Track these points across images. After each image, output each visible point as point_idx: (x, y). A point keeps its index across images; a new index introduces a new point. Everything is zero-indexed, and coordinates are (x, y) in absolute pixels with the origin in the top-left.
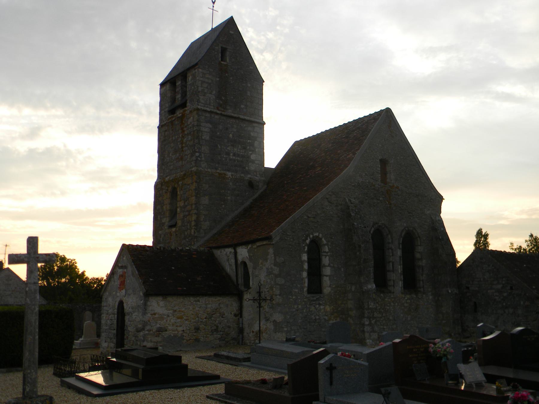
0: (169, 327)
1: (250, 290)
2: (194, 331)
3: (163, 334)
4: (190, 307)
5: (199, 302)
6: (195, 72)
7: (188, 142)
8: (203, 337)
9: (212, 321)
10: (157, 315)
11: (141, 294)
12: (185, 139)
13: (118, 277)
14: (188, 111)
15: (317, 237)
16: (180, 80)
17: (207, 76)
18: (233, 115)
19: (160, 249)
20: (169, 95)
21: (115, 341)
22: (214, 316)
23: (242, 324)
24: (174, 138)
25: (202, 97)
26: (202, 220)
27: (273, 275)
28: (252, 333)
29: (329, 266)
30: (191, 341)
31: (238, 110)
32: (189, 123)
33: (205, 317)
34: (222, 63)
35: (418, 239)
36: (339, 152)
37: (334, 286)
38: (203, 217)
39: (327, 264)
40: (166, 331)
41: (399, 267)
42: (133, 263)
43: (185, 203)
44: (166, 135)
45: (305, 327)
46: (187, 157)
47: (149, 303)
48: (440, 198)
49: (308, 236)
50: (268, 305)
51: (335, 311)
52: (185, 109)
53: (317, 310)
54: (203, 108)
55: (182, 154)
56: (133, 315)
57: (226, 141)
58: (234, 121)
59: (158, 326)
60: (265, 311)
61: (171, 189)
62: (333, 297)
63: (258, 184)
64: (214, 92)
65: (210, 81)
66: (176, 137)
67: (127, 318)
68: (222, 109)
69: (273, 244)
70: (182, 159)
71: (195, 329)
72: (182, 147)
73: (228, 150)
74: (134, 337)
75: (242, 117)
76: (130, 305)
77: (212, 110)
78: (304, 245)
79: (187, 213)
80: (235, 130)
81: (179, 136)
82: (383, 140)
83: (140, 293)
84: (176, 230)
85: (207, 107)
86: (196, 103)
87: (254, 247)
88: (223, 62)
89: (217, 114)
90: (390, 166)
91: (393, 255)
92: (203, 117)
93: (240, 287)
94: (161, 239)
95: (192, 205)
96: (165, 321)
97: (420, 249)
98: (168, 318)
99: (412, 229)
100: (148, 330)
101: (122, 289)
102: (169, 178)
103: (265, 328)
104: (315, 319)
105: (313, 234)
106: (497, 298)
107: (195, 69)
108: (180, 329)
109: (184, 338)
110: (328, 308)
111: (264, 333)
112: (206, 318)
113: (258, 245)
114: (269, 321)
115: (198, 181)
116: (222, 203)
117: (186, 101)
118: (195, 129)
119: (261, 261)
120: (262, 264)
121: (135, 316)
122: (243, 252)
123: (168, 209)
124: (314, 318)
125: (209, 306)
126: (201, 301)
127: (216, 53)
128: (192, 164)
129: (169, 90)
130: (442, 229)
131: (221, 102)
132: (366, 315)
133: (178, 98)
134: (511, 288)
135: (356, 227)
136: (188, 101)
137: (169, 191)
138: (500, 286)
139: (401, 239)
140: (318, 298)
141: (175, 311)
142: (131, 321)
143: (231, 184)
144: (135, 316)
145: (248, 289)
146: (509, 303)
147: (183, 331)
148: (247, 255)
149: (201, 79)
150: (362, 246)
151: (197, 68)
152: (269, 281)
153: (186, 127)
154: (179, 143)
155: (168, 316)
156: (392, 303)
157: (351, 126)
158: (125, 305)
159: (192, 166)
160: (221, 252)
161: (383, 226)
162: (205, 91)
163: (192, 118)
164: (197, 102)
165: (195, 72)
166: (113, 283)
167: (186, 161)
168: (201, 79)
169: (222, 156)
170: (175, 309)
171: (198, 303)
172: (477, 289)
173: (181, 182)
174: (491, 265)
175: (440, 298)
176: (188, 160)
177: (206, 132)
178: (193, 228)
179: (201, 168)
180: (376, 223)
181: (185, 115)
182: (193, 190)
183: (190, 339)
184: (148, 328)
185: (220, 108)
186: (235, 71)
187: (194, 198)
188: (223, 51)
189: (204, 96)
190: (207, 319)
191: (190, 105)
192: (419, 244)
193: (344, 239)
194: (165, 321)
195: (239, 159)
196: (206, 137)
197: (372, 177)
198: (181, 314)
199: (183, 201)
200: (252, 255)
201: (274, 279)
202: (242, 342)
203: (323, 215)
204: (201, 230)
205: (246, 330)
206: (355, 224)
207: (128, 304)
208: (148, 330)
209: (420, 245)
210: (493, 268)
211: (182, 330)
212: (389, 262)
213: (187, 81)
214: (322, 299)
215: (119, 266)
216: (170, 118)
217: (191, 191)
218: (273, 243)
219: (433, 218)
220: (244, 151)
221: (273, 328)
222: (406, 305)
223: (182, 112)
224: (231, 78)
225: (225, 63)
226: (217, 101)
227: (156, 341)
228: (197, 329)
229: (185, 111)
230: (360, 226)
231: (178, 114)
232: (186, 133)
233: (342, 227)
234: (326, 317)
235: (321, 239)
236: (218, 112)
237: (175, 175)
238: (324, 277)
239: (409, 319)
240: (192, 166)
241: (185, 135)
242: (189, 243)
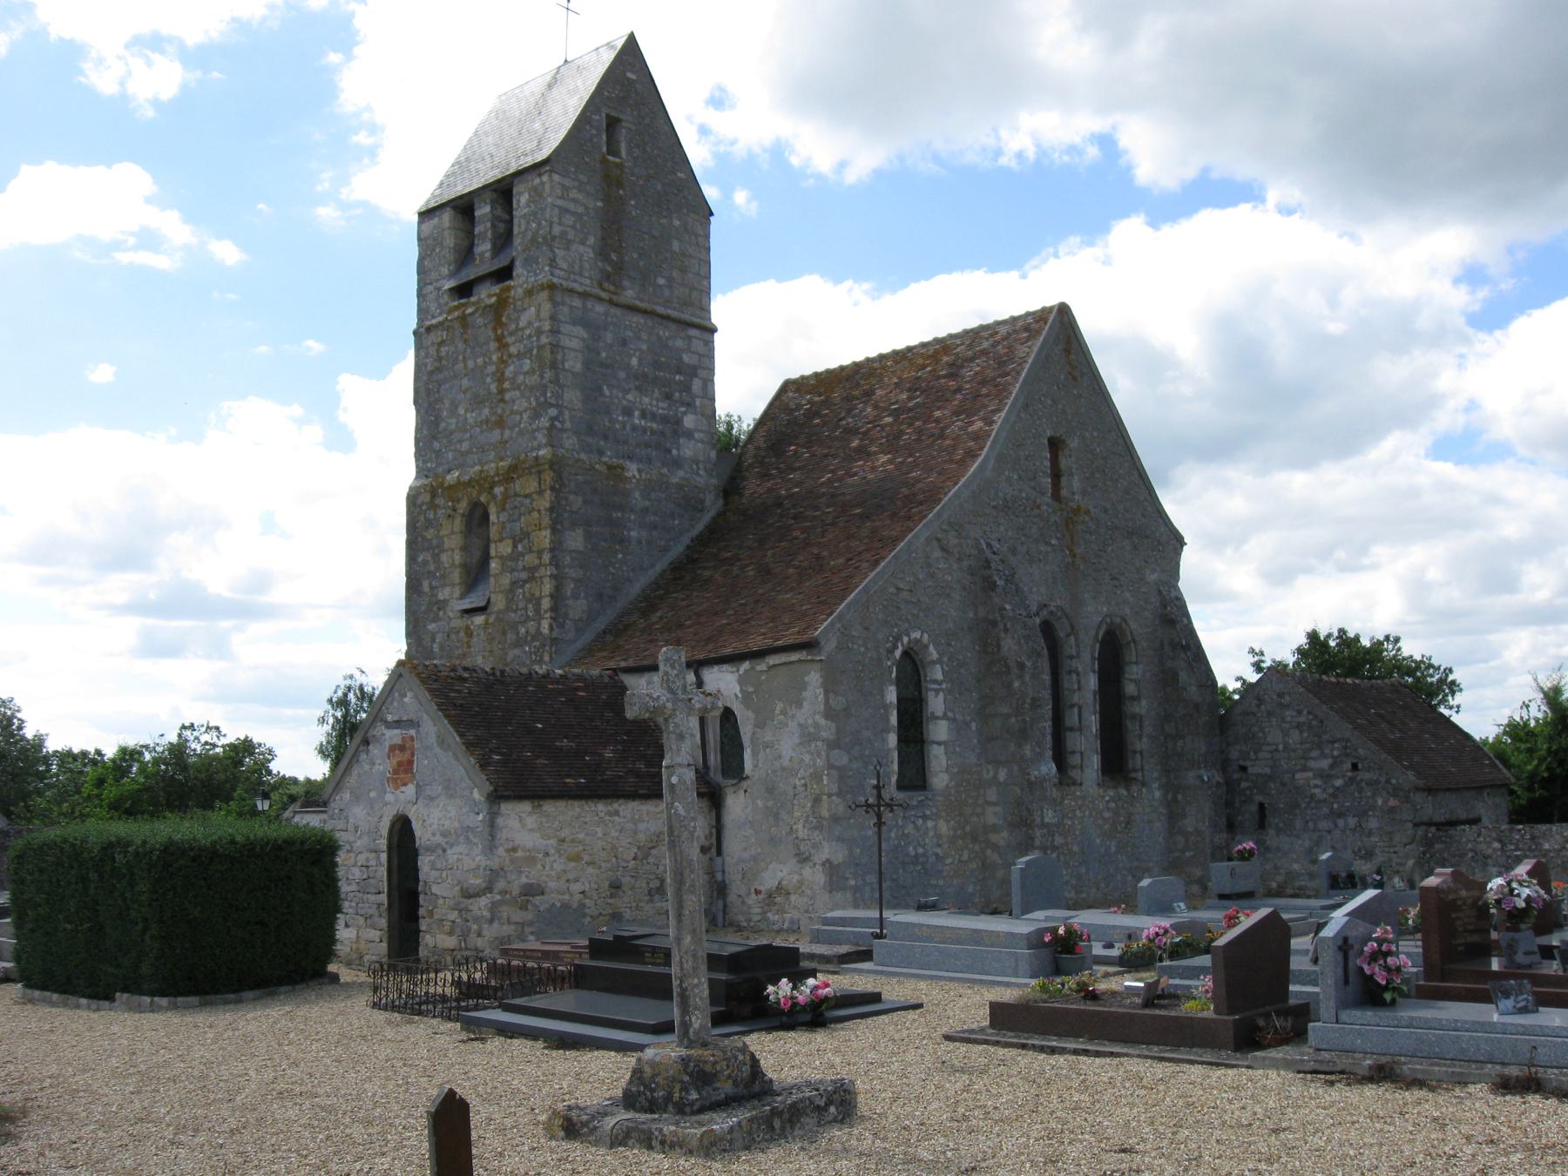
0: (550, 884)
1: (745, 784)
2: (608, 893)
3: (537, 900)
4: (598, 829)
5: (618, 816)
6: (543, 183)
7: (521, 377)
8: (631, 908)
9: (648, 867)
10: (520, 851)
11: (476, 795)
12: (512, 368)
13: (387, 750)
14: (520, 291)
15: (918, 641)
16: (488, 201)
17: (574, 194)
18: (638, 303)
19: (494, 674)
20: (450, 241)
21: (383, 922)
22: (654, 852)
23: (723, 872)
24: (471, 364)
25: (560, 253)
26: (569, 593)
27: (819, 744)
28: (753, 896)
29: (945, 717)
30: (601, 918)
31: (651, 289)
32: (522, 324)
33: (633, 855)
34: (608, 160)
35: (1132, 644)
36: (937, 414)
37: (956, 770)
38: (572, 586)
39: (939, 713)
40: (543, 894)
41: (1093, 717)
42: (440, 713)
43: (515, 546)
44: (444, 354)
45: (894, 876)
46: (518, 417)
47: (500, 821)
48: (1178, 540)
49: (898, 638)
50: (805, 822)
51: (959, 832)
52: (507, 283)
53: (918, 830)
54: (565, 284)
55: (500, 411)
56: (449, 851)
57: (622, 375)
58: (642, 321)
59: (524, 880)
60: (794, 836)
61: (465, 505)
62: (953, 799)
63: (701, 495)
64: (591, 240)
65: (580, 210)
66: (480, 361)
67: (424, 863)
68: (612, 288)
69: (821, 660)
70: (500, 423)
71: (611, 886)
72: (501, 391)
73: (629, 401)
74: (456, 912)
75: (660, 310)
76: (435, 826)
77: (588, 289)
78: (889, 663)
79: (524, 575)
80: (644, 347)
81: (490, 359)
82: (1055, 387)
83: (472, 793)
84: (487, 621)
85: (575, 281)
86: (547, 269)
87: (759, 668)
88: (611, 158)
89: (600, 299)
90: (1070, 456)
91: (1079, 689)
92: (566, 309)
93: (712, 774)
94: (435, 645)
95: (540, 553)
96: (539, 866)
97: (1137, 674)
98: (547, 859)
99: (1118, 620)
100: (500, 893)
101: (405, 784)
102: (458, 477)
103: (798, 881)
104: (917, 856)
105: (908, 636)
106: (1317, 791)
107: (540, 175)
108: (576, 888)
109: (587, 911)
110: (943, 827)
111: (795, 893)
112: (634, 859)
113: (771, 663)
114: (811, 864)
115: (557, 486)
116: (617, 547)
117: (512, 262)
118: (544, 340)
119: (779, 706)
120: (783, 712)
121: (456, 856)
122: (724, 682)
123: (457, 563)
124: (913, 853)
125: (642, 826)
126: (621, 814)
127: (594, 132)
128: (535, 439)
129: (449, 228)
130: (1185, 621)
131: (609, 269)
132: (1037, 843)
133: (483, 253)
134: (1355, 767)
135: (1010, 614)
136: (518, 263)
137: (461, 511)
138: (1325, 764)
139: (1098, 645)
140: (922, 801)
141: (563, 840)
142: (441, 870)
143: (637, 494)
144: (456, 856)
145: (739, 781)
146: (1347, 804)
147: (583, 893)
148: (737, 689)
149: (559, 202)
150: (1028, 664)
151: (546, 171)
152: (807, 758)
153: (511, 334)
154: (488, 380)
155: (547, 854)
156: (1078, 811)
157: (958, 345)
158: (417, 827)
159: (535, 443)
160: (649, 683)
161: (1059, 614)
162: (569, 237)
163: (533, 309)
164: (551, 266)
165: (543, 183)
166: (367, 767)
167: (517, 429)
168: (559, 202)
169: (615, 416)
170: (563, 835)
171: (616, 818)
172: (1267, 770)
173: (502, 489)
174: (1305, 712)
175: (1180, 797)
176: (522, 425)
177: (575, 350)
178: (548, 615)
179: (564, 451)
180: (1045, 605)
181: (511, 300)
182: (543, 512)
183: (600, 914)
184: (501, 885)
185: (606, 285)
186: (641, 182)
187: (547, 533)
188: (612, 124)
189: (568, 249)
190: (638, 862)
191: (525, 273)
192: (1134, 660)
193: (977, 647)
194: (539, 866)
195: (655, 425)
196: (574, 363)
197: (1033, 484)
198: (576, 849)
199: (510, 542)
200: (751, 689)
201: (823, 753)
202: (724, 920)
203: (929, 583)
204: (567, 621)
205: (736, 888)
206: (1008, 607)
207: (428, 822)
208: (504, 892)
209: (1136, 663)
210: (1311, 717)
211: (581, 890)
212: (1072, 706)
213: (515, 206)
214: (931, 804)
215: (386, 722)
216: (456, 308)
217: (535, 514)
218: (823, 658)
219: (1165, 593)
220: (665, 405)
221: (823, 880)
222: (1106, 815)
223: (498, 291)
224: (633, 202)
225: (618, 160)
226: (600, 264)
227: (521, 921)
228: (616, 887)
229: (509, 289)
230: (1018, 612)
231: (482, 296)
232: (513, 350)
233: (971, 615)
234: (939, 851)
235: (926, 647)
236: (603, 295)
237: (478, 468)
238: (935, 746)
239: (1113, 849)
240: (535, 443)
241: (510, 356)
242: (534, 657)
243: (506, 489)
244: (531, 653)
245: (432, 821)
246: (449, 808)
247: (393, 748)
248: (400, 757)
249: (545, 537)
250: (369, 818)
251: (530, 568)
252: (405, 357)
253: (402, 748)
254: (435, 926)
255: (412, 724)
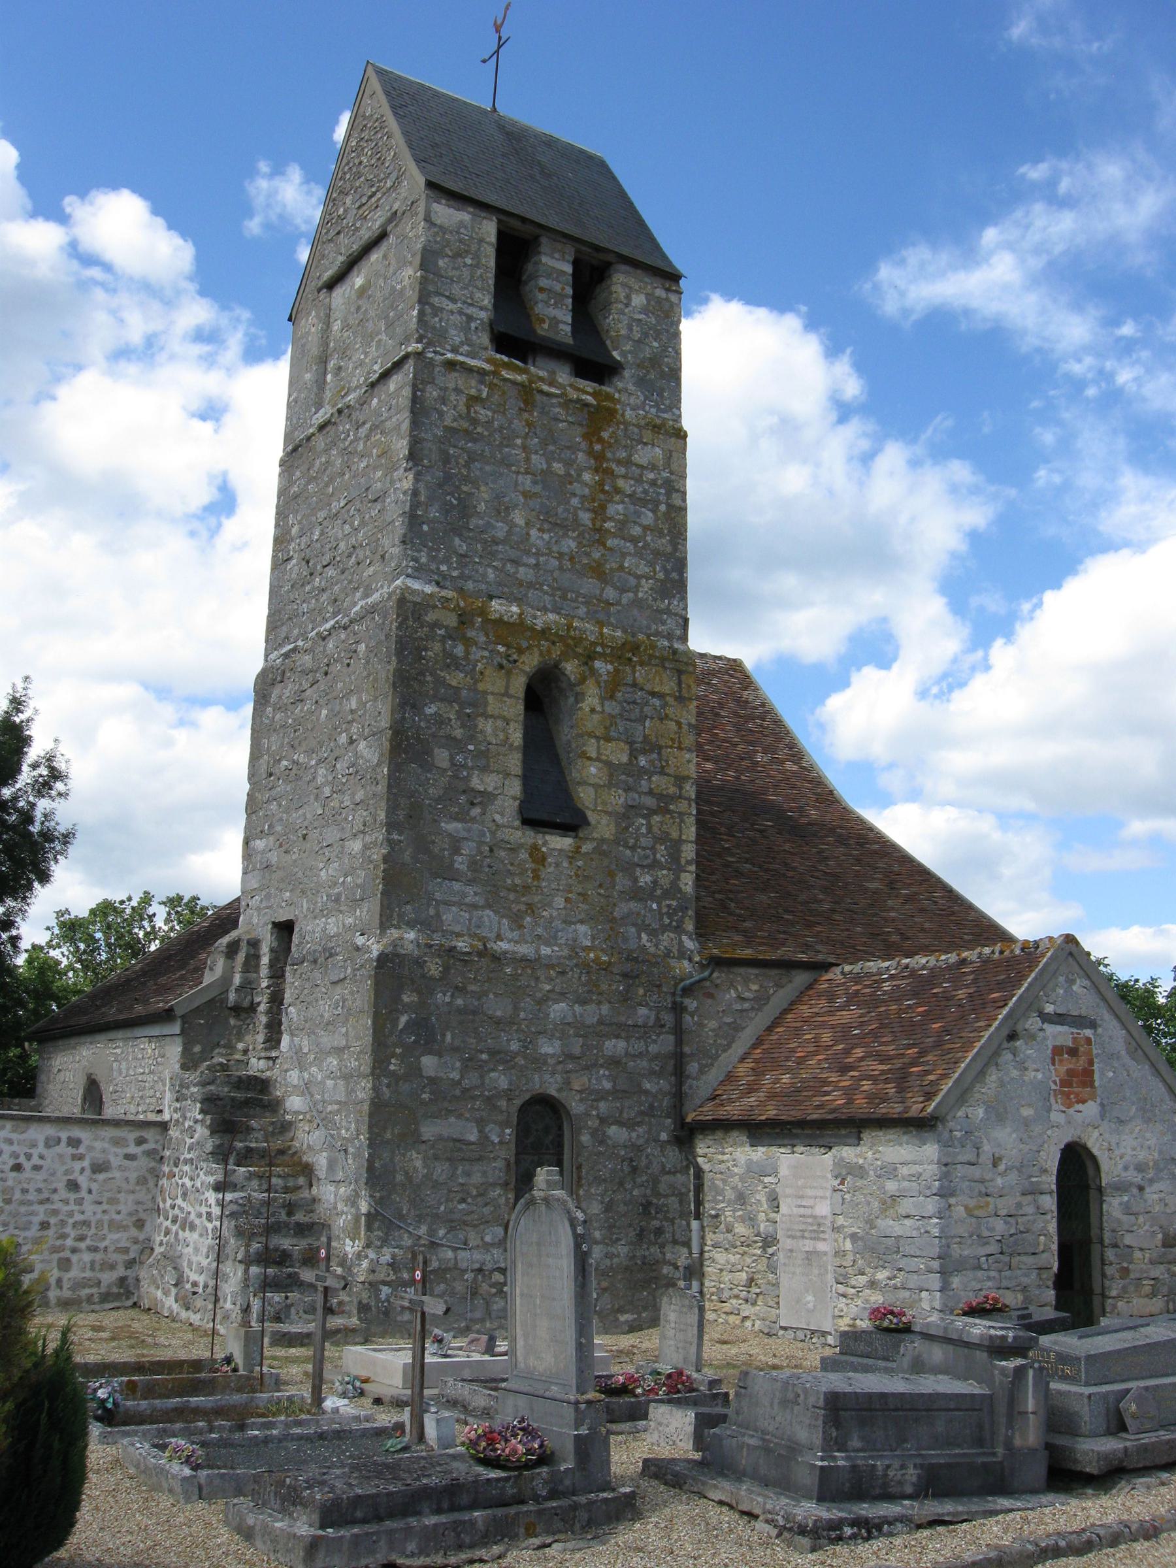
13: (1049, 1052)
84: (578, 849)
101: (1084, 1102)
182: (685, 727)
242: (667, 921)
243: (617, 671)
244: (661, 915)
245: (1122, 1150)
246: (1148, 1135)
247: (1057, 1051)
248: (1067, 1064)
249: (689, 761)
250: (1022, 1146)
251: (661, 795)
252: (284, 353)
253: (1073, 1052)
254: (1131, 1288)
255: (1080, 1021)
